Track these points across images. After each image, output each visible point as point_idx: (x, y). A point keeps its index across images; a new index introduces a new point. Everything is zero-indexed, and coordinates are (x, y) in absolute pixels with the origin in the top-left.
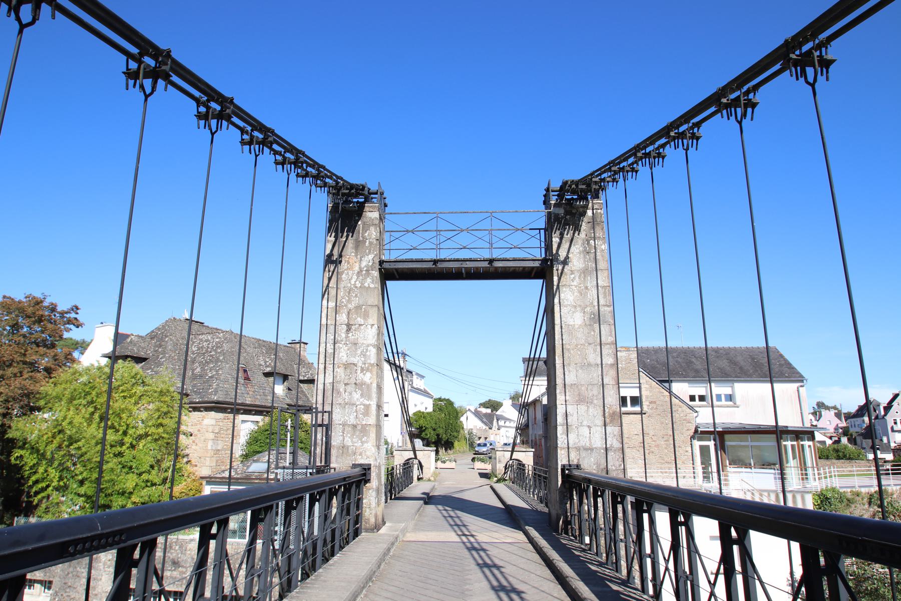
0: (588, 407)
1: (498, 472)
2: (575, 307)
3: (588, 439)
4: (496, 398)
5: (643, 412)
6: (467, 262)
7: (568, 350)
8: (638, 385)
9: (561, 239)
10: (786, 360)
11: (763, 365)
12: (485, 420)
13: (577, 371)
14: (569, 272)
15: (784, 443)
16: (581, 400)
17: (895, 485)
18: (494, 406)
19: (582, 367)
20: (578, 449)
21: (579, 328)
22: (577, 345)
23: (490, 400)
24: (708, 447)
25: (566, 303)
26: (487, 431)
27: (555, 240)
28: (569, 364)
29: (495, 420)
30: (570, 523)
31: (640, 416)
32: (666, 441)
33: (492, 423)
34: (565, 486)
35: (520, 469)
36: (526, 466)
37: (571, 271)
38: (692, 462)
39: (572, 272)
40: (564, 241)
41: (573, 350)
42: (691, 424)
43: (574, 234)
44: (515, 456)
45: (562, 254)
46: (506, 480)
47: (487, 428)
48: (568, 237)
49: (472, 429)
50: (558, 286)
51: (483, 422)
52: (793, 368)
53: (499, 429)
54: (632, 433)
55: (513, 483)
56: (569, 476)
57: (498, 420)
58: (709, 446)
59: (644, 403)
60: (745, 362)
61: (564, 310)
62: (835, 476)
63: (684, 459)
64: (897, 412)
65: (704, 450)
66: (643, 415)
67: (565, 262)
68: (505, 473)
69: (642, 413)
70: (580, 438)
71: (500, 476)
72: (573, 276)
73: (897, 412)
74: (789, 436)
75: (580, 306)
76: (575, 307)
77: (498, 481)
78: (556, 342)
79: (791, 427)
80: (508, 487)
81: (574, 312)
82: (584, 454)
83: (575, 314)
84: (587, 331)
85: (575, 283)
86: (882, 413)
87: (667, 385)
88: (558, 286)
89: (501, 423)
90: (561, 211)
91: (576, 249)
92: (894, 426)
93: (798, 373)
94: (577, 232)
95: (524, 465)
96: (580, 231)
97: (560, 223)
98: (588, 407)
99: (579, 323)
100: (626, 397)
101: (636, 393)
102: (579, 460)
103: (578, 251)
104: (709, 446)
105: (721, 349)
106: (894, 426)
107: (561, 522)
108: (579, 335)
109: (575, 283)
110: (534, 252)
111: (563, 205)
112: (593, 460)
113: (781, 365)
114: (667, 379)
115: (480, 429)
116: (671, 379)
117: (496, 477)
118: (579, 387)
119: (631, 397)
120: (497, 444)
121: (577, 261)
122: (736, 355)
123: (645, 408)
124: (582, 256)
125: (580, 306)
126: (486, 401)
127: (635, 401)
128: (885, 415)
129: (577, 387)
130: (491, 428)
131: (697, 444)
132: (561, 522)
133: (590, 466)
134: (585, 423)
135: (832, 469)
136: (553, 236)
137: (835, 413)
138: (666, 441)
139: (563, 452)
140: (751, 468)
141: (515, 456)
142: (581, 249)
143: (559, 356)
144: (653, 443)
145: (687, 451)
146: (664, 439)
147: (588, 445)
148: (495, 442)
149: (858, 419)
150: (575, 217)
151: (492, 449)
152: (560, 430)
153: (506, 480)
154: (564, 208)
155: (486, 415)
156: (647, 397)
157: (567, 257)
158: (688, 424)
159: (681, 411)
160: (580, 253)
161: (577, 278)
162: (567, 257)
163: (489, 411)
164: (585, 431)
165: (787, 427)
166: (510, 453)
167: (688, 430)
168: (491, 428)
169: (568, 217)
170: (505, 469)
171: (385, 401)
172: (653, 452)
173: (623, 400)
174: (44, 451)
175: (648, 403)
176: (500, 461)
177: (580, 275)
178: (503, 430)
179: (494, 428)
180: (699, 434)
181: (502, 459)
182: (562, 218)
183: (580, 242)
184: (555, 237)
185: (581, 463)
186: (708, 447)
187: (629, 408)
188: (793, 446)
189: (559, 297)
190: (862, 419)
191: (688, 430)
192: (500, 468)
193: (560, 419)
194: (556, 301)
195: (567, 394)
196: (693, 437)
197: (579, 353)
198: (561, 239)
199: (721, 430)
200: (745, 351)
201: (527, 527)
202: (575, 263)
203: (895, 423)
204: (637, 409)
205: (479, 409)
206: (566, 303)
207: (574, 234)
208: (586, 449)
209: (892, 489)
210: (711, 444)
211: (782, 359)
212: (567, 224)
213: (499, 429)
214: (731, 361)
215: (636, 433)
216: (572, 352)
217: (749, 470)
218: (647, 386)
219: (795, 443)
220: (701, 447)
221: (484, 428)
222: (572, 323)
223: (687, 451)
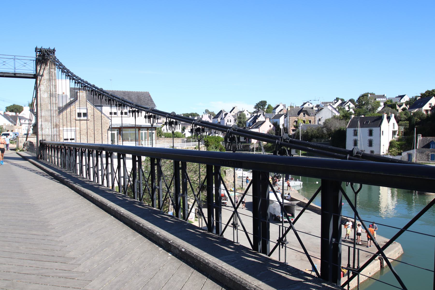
0: (48, 123)
1: (20, 147)
2: (45, 91)
3: (48, 132)
4: (18, 103)
5: (88, 119)
6: (6, 74)
7: (42, 105)
8: (86, 108)
9: (41, 68)
10: (151, 98)
11: (142, 100)
12: (11, 120)
13: (45, 112)
14: (43, 80)
15: (141, 132)
16: (46, 121)
17: (180, 146)
18: (16, 109)
19: (47, 111)
20: (45, 135)
21: (46, 98)
22: (45, 104)
23: (14, 105)
24: (114, 134)
25: (42, 90)
26: (12, 126)
27: (38, 68)
28: (42, 110)
29: (18, 120)
30: (42, 156)
31: (86, 121)
32: (97, 132)
33: (16, 121)
34: (41, 146)
35: (31, 144)
36: (34, 143)
37: (44, 79)
38: (107, 140)
39: (44, 80)
40: (41, 69)
41: (44, 105)
42: (108, 125)
43: (45, 67)
44: (29, 139)
45: (41, 73)
46: (24, 151)
47: (13, 125)
48: (43, 67)
49: (2, 126)
50: (39, 84)
51: (10, 121)
52: (153, 102)
53: (21, 125)
54: (83, 128)
55: (27, 151)
56: (42, 143)
57: (20, 120)
58: (115, 133)
59: (88, 116)
60: (135, 98)
61: (41, 92)
62: (158, 143)
63: (104, 139)
64: (229, 116)
65: (113, 135)
66: (88, 121)
67: (42, 76)
68: (23, 148)
69: (87, 120)
70: (46, 132)
71: (21, 149)
72: (44, 81)
73: (229, 116)
74: (144, 129)
75: (46, 91)
76: (45, 91)
77: (21, 151)
78: (38, 103)
79: (143, 125)
80: (26, 153)
81: (44, 93)
82: (47, 137)
83: (45, 94)
84: (49, 99)
85: (45, 83)
86: (224, 116)
87: (99, 108)
88: (39, 84)
89: (23, 121)
90: (41, 58)
91: (46, 72)
92: (227, 123)
93: (154, 104)
94: (46, 66)
95: (32, 143)
96: (47, 66)
97: (40, 62)
98: (48, 123)
99: (46, 97)
100: (81, 113)
101: (85, 112)
102: (45, 138)
103: (46, 72)
104: (115, 133)
105: (126, 92)
106: (227, 123)
107: (39, 156)
108: (46, 100)
109: (45, 83)
110: (32, 71)
111: (41, 56)
112: (49, 138)
113: (148, 100)
114: (100, 105)
115: (8, 126)
116: (102, 105)
117: (19, 149)
118: (46, 117)
119: (83, 113)
120: (20, 134)
121: (46, 76)
122: (132, 95)
123: (89, 118)
124: (48, 74)
125: (46, 91)
126: (11, 106)
127: (85, 115)
128: (224, 118)
129: (45, 116)
130: (15, 125)
131: (110, 132)
132: (39, 156)
133: (48, 140)
134: (47, 128)
135: (157, 141)
136: (38, 66)
137: (209, 116)
138: (97, 132)
139: (40, 136)
140: (129, 141)
141: (29, 139)
142: (47, 72)
143: (39, 107)
144: (92, 132)
145: (106, 136)
146: (96, 131)
147: (48, 134)
148: (18, 133)
149: (216, 119)
150: (45, 60)
151: (16, 137)
152: (39, 130)
153: (24, 151)
154: (42, 57)
155: (12, 117)
156: (90, 113)
157: (43, 74)
158: (107, 125)
159: (105, 119)
160: (47, 73)
161: (46, 82)
162: (43, 74)
163: (14, 114)
164: (47, 130)
165: (141, 126)
166: (26, 138)
167: (106, 127)
168: (15, 125)
169: (43, 60)
170: (24, 145)
171: (342, 237)
172: (91, 136)
173: (79, 115)
174: (414, 121)
175: (90, 116)
176: (21, 142)
177: (47, 81)
178: (23, 125)
179: (17, 125)
180: (112, 128)
181: (22, 141)
182: (41, 60)
183: (47, 70)
184: (38, 67)
185: (46, 139)
186: (114, 134)
187: (82, 118)
188: (145, 133)
189: (40, 88)
190: (217, 119)
191: (106, 127)
192: (21, 145)
193: (39, 126)
194: (39, 89)
195: (42, 119)
196: (108, 130)
197: (46, 106)
198: (41, 68)
199: (119, 127)
200: (136, 93)
201: (29, 159)
202: (45, 77)
203: (228, 121)
204: (85, 118)
205: (7, 113)
206: (42, 90)
207: (45, 67)
208: (47, 135)
209: (178, 148)
210: (115, 132)
211: (150, 98)
212: (43, 63)
213: (21, 125)
214: (129, 98)
215: (84, 128)
216: (43, 106)
217: (128, 142)
218: (90, 108)
219: (147, 132)
220: (112, 134)
221: (11, 125)
222: (43, 97)
223: (106, 136)
